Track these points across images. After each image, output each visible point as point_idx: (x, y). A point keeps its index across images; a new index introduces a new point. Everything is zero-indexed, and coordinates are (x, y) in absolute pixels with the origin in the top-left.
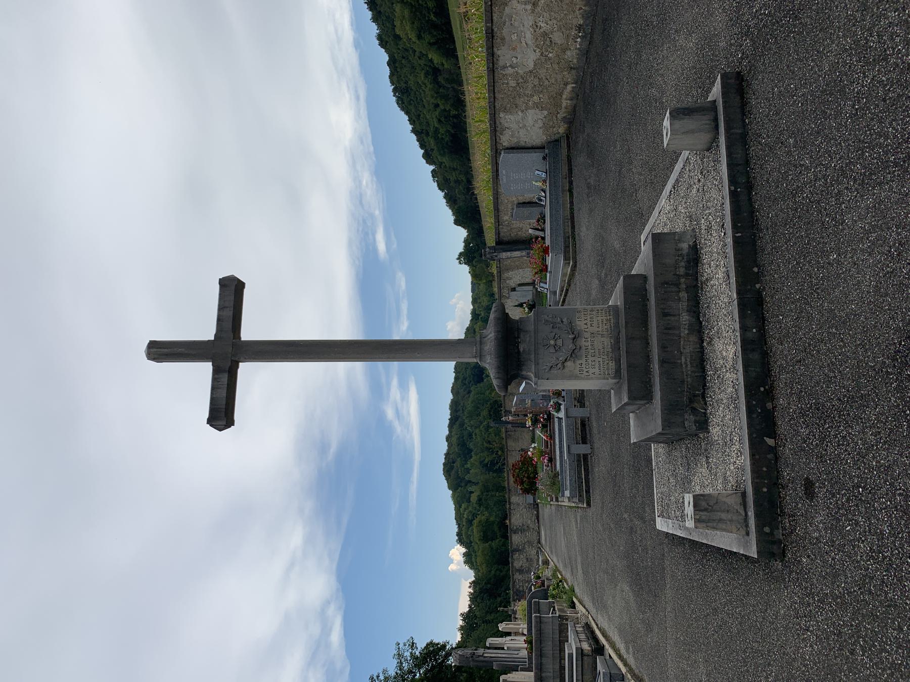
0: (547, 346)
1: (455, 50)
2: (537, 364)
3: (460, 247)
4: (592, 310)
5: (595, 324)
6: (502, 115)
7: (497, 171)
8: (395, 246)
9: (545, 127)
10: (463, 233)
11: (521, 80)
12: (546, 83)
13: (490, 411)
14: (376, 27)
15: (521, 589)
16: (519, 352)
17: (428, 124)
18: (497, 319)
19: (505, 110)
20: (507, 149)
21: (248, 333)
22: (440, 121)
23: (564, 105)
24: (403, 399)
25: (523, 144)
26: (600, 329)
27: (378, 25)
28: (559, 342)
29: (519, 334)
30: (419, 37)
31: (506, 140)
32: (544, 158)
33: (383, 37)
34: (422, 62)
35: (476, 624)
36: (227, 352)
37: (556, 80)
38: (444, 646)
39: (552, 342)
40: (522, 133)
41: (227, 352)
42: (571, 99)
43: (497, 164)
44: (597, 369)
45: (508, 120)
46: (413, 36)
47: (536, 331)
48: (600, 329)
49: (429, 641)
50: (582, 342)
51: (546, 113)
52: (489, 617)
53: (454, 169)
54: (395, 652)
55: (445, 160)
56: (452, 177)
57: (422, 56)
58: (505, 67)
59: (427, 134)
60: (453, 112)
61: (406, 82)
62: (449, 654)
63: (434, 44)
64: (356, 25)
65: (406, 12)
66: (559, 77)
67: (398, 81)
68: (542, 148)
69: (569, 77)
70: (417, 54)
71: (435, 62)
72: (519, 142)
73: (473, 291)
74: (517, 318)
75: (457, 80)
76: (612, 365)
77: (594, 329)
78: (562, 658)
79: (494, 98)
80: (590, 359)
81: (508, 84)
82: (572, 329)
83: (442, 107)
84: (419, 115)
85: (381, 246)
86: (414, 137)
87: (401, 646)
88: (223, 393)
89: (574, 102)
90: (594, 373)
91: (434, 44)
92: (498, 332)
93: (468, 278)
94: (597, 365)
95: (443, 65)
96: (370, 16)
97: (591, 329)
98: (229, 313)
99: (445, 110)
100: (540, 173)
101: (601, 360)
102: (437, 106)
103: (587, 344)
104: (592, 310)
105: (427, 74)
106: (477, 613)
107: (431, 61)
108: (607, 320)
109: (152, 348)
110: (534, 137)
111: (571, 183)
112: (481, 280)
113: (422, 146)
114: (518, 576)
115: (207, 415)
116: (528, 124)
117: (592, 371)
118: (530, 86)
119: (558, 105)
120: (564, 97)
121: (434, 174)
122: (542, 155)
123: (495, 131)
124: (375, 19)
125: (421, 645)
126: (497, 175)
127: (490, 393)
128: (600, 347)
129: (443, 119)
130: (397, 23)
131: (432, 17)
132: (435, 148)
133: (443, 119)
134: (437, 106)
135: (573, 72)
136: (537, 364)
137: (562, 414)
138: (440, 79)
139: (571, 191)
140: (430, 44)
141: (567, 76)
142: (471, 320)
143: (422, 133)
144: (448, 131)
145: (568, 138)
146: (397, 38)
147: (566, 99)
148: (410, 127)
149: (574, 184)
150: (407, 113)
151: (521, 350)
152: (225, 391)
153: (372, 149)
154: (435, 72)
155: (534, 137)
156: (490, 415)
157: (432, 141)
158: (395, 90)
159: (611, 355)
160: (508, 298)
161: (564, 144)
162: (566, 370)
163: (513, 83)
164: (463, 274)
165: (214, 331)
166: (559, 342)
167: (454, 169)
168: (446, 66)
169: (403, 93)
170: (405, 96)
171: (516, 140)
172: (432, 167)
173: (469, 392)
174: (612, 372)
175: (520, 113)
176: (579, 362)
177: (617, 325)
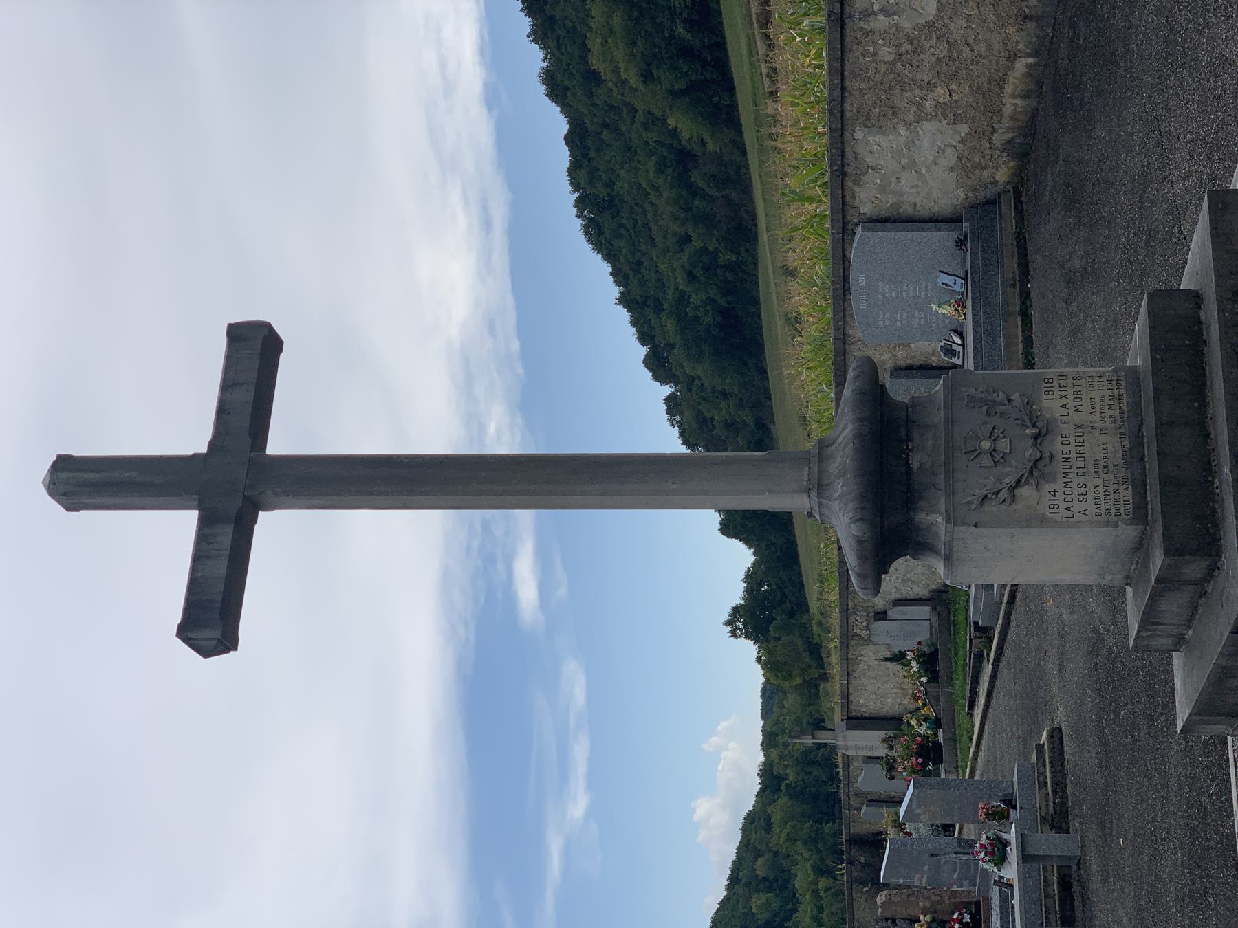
0: (976, 453)
1: (733, 107)
2: (951, 493)
3: (735, 593)
5: (1085, 407)
6: (859, 134)
7: (845, 279)
8: (562, 591)
9: (964, 166)
10: (741, 556)
11: (906, 47)
12: (967, 53)
14: (541, 55)
17: (661, 284)
18: (860, 394)
19: (867, 123)
20: (871, 220)
21: (282, 440)
22: (691, 276)
23: (1008, 109)
25: (910, 210)
27: (545, 48)
28: (1003, 445)
29: (908, 433)
30: (647, 77)
31: (866, 199)
32: (961, 243)
33: (559, 77)
34: (652, 136)
36: (234, 482)
37: (989, 47)
39: (986, 445)
40: (908, 179)
41: (234, 482)
42: (1026, 95)
43: (845, 259)
44: (1091, 501)
45: (874, 146)
46: (631, 75)
48: (1097, 417)
50: (1057, 445)
51: (964, 129)
53: (725, 395)
55: (703, 371)
56: (719, 413)
57: (652, 121)
58: (869, 13)
59: (659, 308)
60: (726, 257)
61: (610, 185)
63: (683, 92)
64: (493, 51)
65: (617, 20)
66: (996, 39)
67: (591, 182)
68: (955, 220)
69: (1020, 38)
70: (640, 117)
71: (685, 135)
72: (898, 205)
73: (766, 714)
74: (906, 399)
75: (734, 177)
76: (1126, 494)
77: (1084, 417)
79: (843, 89)
80: (1075, 481)
81: (875, 54)
83: (698, 244)
84: (640, 263)
85: (527, 591)
86: (624, 315)
88: (220, 568)
89: (1033, 102)
90: (1083, 512)
91: (683, 92)
93: (756, 677)
94: (1091, 496)
95: (703, 143)
96: (528, 30)
97: (1075, 417)
98: (245, 396)
99: (705, 251)
100: (949, 280)
101: (1099, 482)
102: (685, 240)
103: (1066, 449)
104: (1078, 377)
105: (661, 168)
107: (674, 133)
109: (63, 470)
110: (936, 194)
111: (1026, 296)
112: (789, 677)
113: (643, 338)
115: (178, 618)
116: (922, 160)
117: (1077, 507)
118: (928, 59)
119: (993, 110)
120: (1009, 89)
121: (672, 404)
122: (955, 235)
123: (844, 174)
124: (540, 35)
126: (845, 290)
128: (1099, 456)
129: (698, 272)
130: (595, 44)
131: (680, 29)
132: (678, 341)
133: (698, 272)
134: (685, 240)
135: (1031, 26)
137: (1011, 872)
138: (695, 177)
139: (1025, 315)
140: (673, 94)
141: (1016, 37)
142: (760, 794)
143: (645, 304)
144: (711, 301)
145: (1017, 193)
146: (593, 78)
147: (1013, 96)
148: (616, 291)
149: (1034, 295)
150: (609, 256)
151: (915, 466)
152: (226, 562)
153: (516, 346)
154: (682, 159)
155: (936, 194)
157: (670, 325)
158: (580, 204)
160: (868, 641)
161: (1008, 209)
162: (1018, 506)
163: (886, 54)
164: (742, 667)
165: (208, 435)
166: (1003, 445)
167: (725, 395)
168: (710, 146)
169: (601, 211)
170: (607, 218)
171: (891, 200)
172: (667, 390)
174: (1126, 509)
175: (902, 130)
176: (1048, 487)
177: (1136, 406)
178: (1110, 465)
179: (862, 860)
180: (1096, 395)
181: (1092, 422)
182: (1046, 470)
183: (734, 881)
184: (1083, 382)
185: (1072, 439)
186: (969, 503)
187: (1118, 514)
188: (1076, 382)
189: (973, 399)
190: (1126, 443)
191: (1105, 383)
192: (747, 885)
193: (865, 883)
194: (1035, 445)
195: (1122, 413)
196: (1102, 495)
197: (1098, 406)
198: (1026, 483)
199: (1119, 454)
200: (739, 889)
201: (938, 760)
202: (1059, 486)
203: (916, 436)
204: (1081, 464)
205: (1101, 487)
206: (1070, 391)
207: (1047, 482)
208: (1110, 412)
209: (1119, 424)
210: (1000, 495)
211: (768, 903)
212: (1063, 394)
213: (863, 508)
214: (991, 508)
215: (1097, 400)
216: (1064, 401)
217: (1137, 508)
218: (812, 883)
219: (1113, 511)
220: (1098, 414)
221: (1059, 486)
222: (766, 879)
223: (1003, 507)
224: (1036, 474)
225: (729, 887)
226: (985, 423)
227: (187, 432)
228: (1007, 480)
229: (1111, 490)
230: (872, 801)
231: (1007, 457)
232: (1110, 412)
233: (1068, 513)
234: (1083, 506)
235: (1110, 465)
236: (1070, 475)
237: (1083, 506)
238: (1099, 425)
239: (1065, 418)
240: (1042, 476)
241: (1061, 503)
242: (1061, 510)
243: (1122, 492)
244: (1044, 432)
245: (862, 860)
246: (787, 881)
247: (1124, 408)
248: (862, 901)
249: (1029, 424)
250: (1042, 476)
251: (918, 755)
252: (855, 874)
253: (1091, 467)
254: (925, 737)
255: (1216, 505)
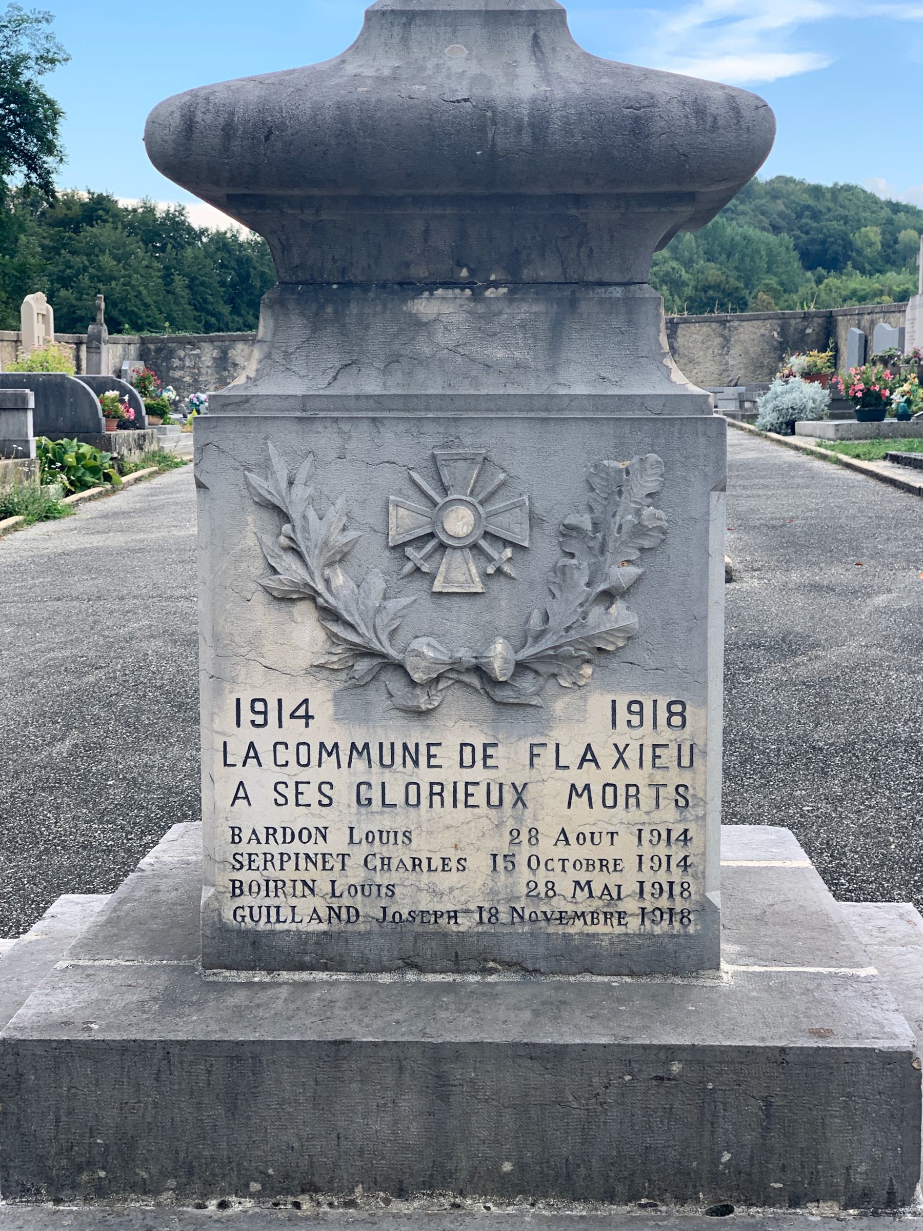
0: (437, 493)
2: (307, 413)
4: (683, 799)
5: (582, 816)
13: (717, 287)
15: (176, 363)
16: (410, 287)
24: (765, 35)
26: (547, 848)
28: (460, 573)
35: (163, 249)
38: (49, 148)
39: (459, 523)
47: (546, 413)
48: (547, 848)
49: (61, 105)
50: (458, 726)
52: (180, 282)
54: (26, 11)
62: (31, 162)
77: (550, 808)
82: (551, 663)
87: (43, 25)
90: (241, 793)
92: (539, 123)
97: (549, 789)
101: (337, 842)
103: (447, 755)
104: (683, 799)
106: (189, 251)
108: (613, 895)
114: (208, 354)
117: (261, 781)
125: (48, 84)
127: (769, 289)
128: (421, 847)
136: (307, 413)
151: (424, 307)
156: (705, 289)
159: (370, 908)
162: (261, 615)
166: (460, 573)
173: (776, 229)
176: (322, 701)
178: (393, 877)
179: (809, 331)
180: (625, 849)
181: (534, 834)
182: (376, 696)
183: (896, 208)
184: (668, 815)
185: (478, 773)
186: (265, 467)
187: (237, 889)
188: (668, 793)
189: (618, 488)
190: (465, 923)
191: (662, 877)
192: (890, 222)
193: (782, 333)
194: (455, 667)
195: (561, 917)
196: (297, 847)
197: (587, 851)
198: (333, 637)
199: (426, 903)
200: (886, 213)
201: (862, 417)
203: (528, 309)
204: (395, 795)
205: (322, 847)
207: (337, 699)
208: (565, 886)
210: (290, 560)
211: (871, 244)
212: (631, 756)
213: (228, 130)
214: (254, 532)
216: (606, 756)
217: (255, 940)
218: (891, 289)
219: (245, 876)
220: (561, 851)
222: (896, 241)
223: (258, 567)
224: (362, 666)
225: (889, 204)
226: (534, 520)
228: (339, 579)
230: (866, 341)
231: (419, 584)
232: (565, 886)
233: (237, 752)
235: (393, 877)
236: (359, 764)
238: (524, 852)
242: (248, 733)
243: (304, 906)
245: (809, 331)
246: (894, 263)
248: (762, 331)
250: (358, 686)
251: (867, 393)
252: (793, 322)
253: (386, 822)
254: (889, 402)
255: (166, 1197)
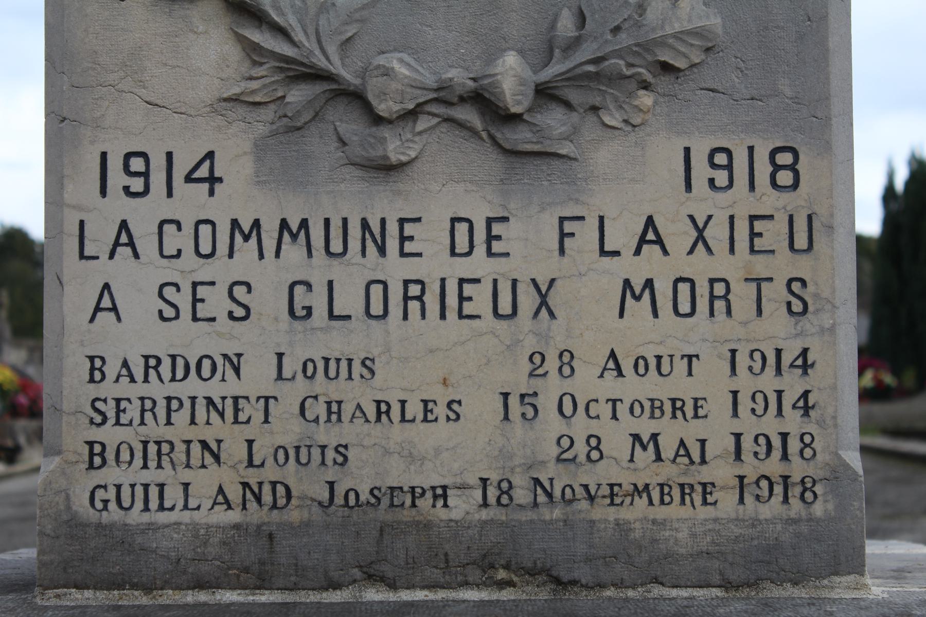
5: (642, 332)
44: (163, 340)
48: (588, 382)
50: (448, 186)
77: (590, 317)
78: (65, 587)
80: (266, 276)
90: (106, 303)
94: (190, 339)
97: (587, 290)
101: (257, 377)
103: (430, 237)
108: (693, 454)
128: (390, 383)
159: (309, 484)
178: (347, 432)
180: (711, 382)
181: (567, 358)
185: (478, 264)
188: (775, 293)
190: (461, 506)
191: (771, 426)
194: (444, 95)
196: (193, 386)
197: (651, 387)
198: (253, 51)
199: (397, 474)
202: (242, 196)
204: (349, 300)
205: (233, 387)
206: (723, 264)
207: (260, 149)
208: (616, 441)
209: (560, 478)
212: (717, 233)
215: (678, 385)
216: (678, 235)
219: (110, 435)
220: (610, 386)
221: (242, 196)
224: (298, 95)
227: (726, 172)
229: (217, 429)
232: (616, 441)
233: (101, 236)
234: (137, 302)
236: (293, 252)
237: (137, 302)
238: (551, 389)
239: (587, 234)
240: (291, 128)
241: (156, 206)
242: (119, 207)
243: (205, 482)
244: (519, 137)
247: (637, 511)
249: (555, 69)
250: (291, 128)
